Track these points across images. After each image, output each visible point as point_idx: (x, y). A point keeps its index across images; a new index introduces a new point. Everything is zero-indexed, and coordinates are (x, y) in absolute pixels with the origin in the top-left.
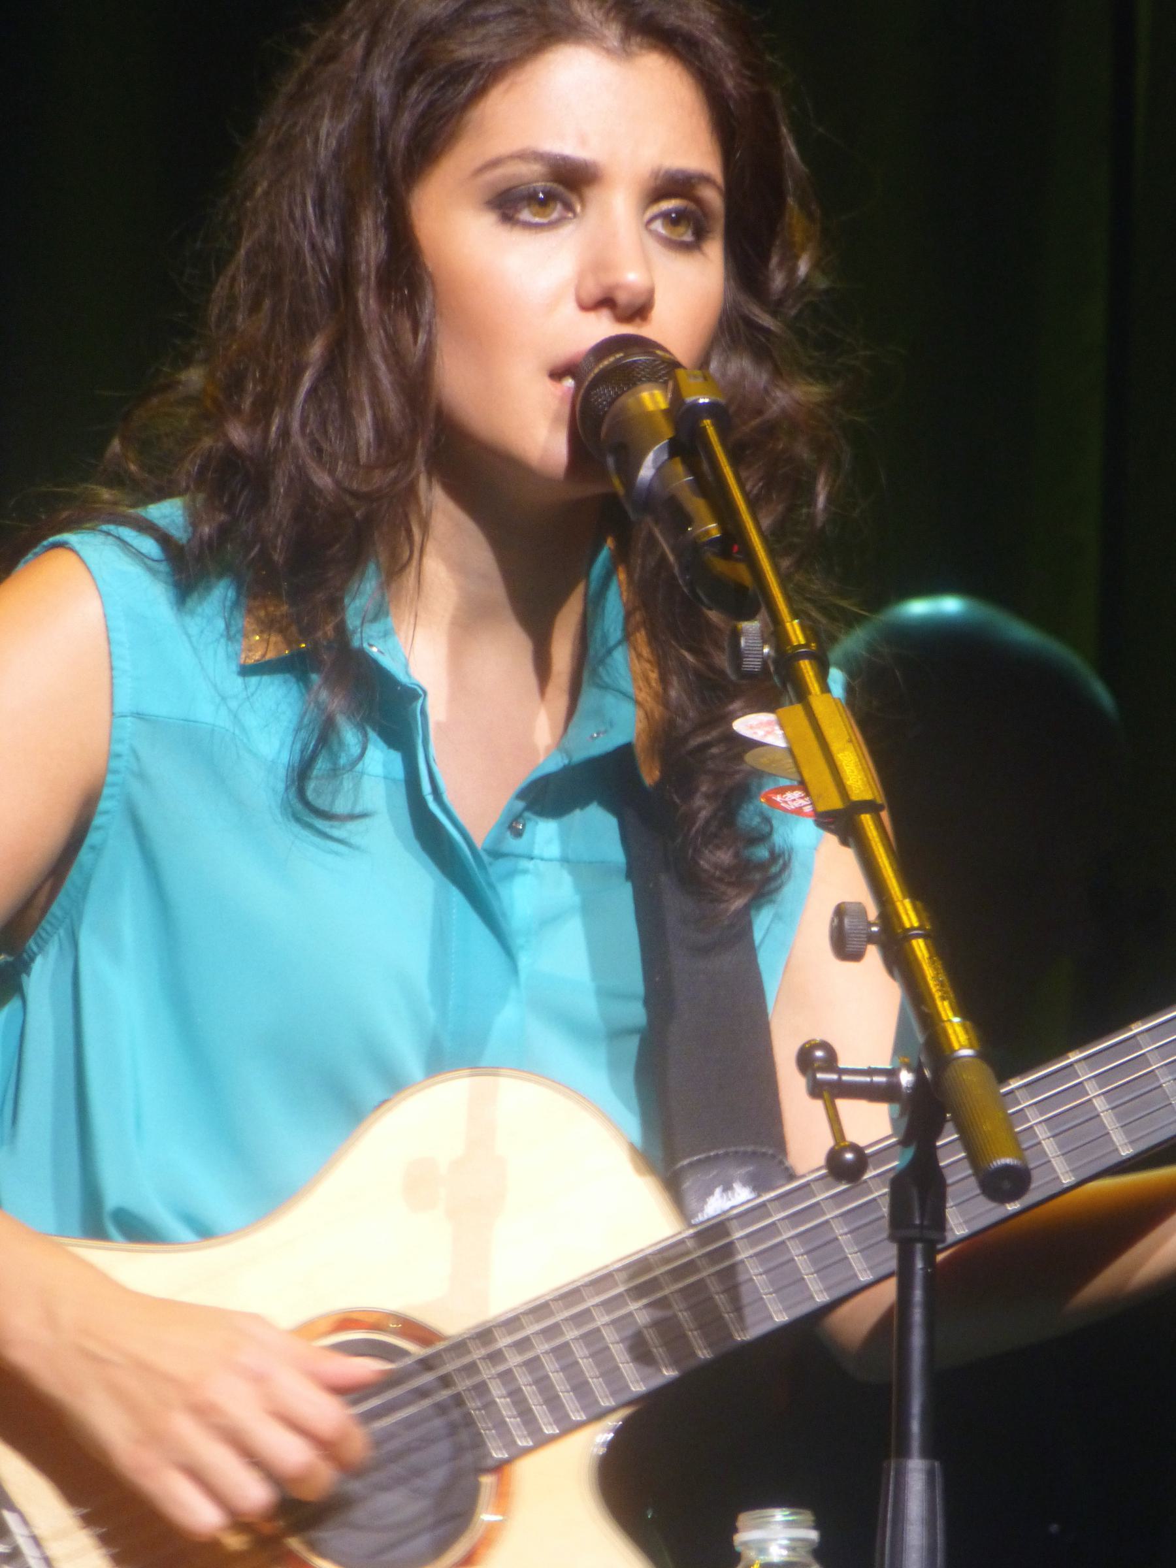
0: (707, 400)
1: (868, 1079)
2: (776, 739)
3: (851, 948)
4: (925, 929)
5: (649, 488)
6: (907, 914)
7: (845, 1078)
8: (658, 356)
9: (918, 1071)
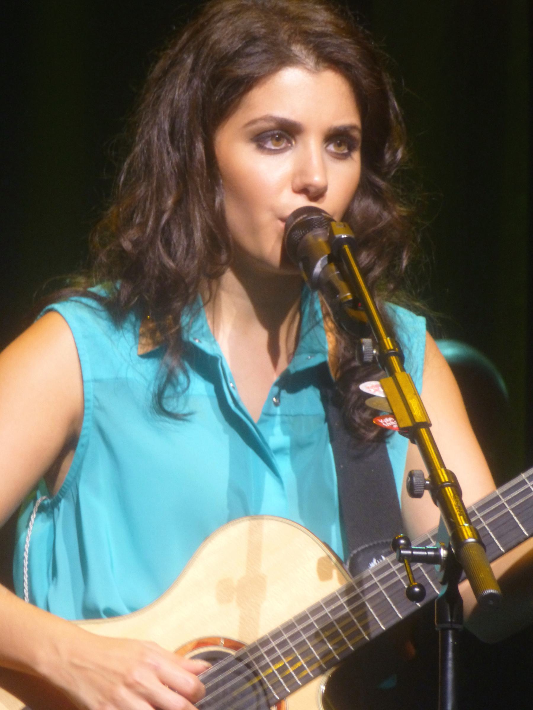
0: (345, 236)
1: (425, 553)
2: (380, 393)
3: (417, 491)
4: (451, 483)
5: (319, 278)
6: (443, 476)
7: (415, 553)
8: (323, 216)
9: (448, 549)
